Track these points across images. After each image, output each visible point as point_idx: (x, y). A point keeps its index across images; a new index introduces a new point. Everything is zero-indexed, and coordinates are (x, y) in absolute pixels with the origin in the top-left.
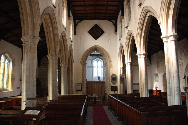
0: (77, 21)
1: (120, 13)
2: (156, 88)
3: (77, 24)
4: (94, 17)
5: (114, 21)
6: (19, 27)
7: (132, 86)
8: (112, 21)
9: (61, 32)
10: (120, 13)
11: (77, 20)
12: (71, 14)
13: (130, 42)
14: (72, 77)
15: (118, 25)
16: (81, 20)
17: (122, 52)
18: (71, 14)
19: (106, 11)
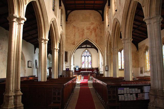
0: (68, 11)
1: (107, 4)
2: (75, 69)
3: (69, 14)
4: (84, 7)
5: (101, 11)
6: (9, 28)
7: (53, 66)
8: (100, 11)
9: (50, 21)
10: (107, 4)
11: (69, 10)
12: (62, 4)
13: (62, 59)
14: (41, 61)
15: (107, 12)
16: (72, 10)
17: (120, 34)
18: (62, 4)
19: (94, 2)
